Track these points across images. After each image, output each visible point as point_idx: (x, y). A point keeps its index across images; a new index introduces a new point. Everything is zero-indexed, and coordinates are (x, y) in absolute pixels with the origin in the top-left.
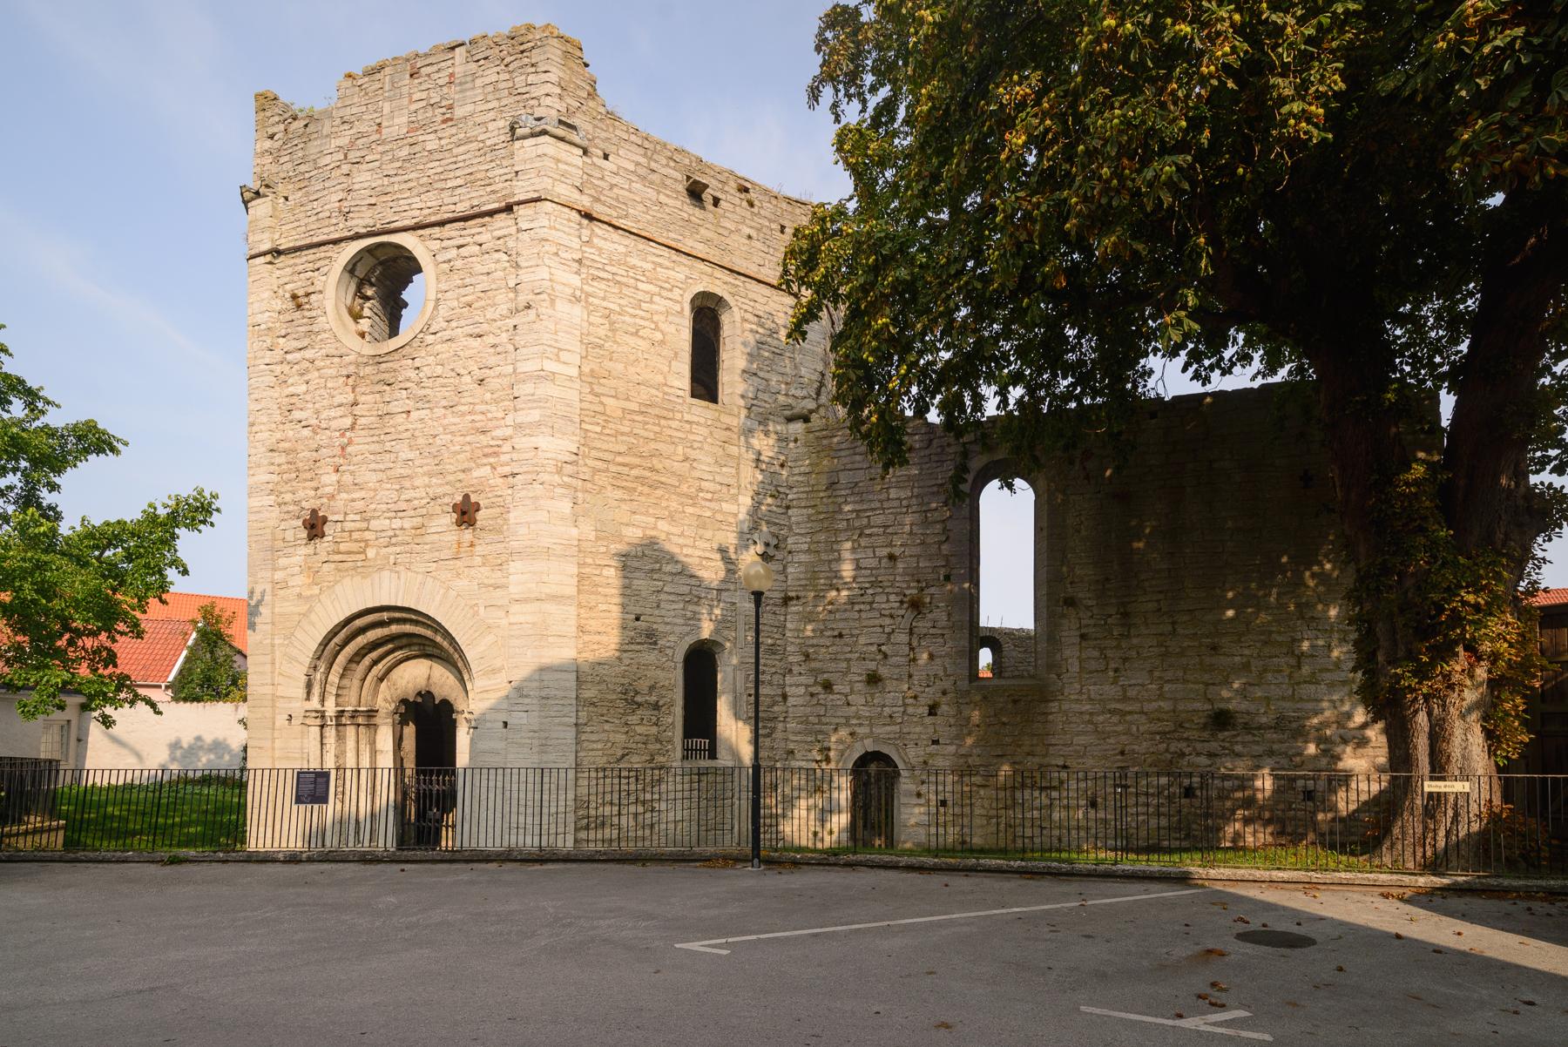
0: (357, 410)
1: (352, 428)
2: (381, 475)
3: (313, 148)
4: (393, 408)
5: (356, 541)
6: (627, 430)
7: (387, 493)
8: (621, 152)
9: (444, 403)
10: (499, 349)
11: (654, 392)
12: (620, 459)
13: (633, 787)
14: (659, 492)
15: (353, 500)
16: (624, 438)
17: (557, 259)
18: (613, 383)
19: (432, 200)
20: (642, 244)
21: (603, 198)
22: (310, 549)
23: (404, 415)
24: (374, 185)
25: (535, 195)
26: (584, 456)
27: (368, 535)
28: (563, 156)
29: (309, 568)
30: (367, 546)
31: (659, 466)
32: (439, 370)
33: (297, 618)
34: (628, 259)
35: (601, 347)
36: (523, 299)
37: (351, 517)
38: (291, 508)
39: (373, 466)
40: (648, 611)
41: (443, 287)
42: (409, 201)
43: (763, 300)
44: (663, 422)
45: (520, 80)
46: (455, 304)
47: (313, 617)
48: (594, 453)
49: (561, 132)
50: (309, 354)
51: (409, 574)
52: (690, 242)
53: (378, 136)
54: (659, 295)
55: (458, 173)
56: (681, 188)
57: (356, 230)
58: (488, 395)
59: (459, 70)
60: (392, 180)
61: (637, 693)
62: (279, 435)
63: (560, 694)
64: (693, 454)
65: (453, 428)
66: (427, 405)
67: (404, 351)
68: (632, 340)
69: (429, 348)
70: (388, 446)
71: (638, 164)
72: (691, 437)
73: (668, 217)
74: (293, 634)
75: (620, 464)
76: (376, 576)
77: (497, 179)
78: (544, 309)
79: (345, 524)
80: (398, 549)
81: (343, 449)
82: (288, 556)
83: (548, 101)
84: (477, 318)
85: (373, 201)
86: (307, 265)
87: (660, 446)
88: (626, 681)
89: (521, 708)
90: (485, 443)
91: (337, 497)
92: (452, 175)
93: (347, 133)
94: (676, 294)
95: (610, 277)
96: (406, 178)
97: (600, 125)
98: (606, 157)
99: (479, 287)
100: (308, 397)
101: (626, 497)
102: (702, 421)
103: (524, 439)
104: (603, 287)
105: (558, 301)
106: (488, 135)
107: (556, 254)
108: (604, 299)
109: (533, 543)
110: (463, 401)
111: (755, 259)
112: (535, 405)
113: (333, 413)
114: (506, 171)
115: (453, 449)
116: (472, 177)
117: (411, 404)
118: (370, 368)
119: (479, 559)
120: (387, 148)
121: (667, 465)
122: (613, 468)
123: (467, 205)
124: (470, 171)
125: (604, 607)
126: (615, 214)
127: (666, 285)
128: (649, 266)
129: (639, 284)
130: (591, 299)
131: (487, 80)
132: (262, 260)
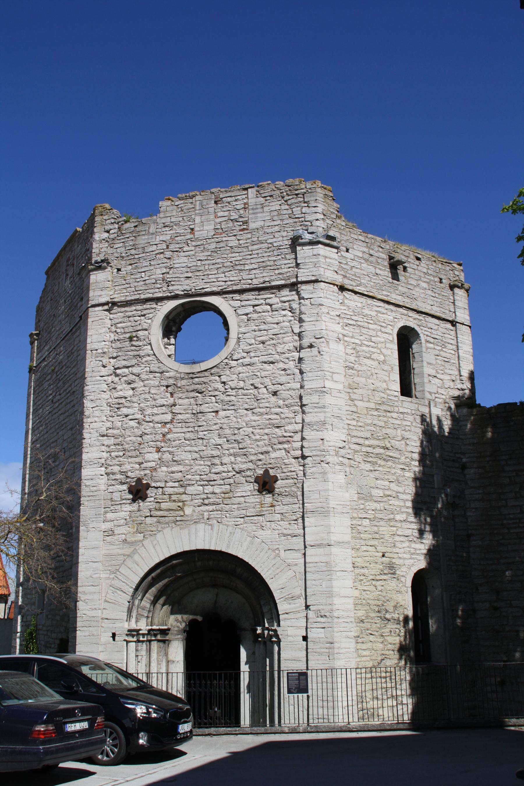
0: (176, 409)
1: (172, 421)
2: (196, 455)
3: (142, 240)
4: (204, 408)
5: (174, 501)
6: (370, 422)
7: (201, 467)
8: (355, 247)
9: (246, 406)
10: (288, 372)
11: (383, 395)
12: (367, 442)
13: (389, 685)
14: (390, 463)
15: (173, 472)
16: (369, 428)
17: (328, 316)
18: (360, 391)
19: (233, 276)
20: (370, 301)
21: (348, 275)
22: (135, 506)
23: (214, 414)
24: (189, 265)
25: (313, 278)
26: (349, 442)
27: (184, 497)
28: (328, 254)
29: (133, 521)
30: (184, 505)
31: (388, 445)
32: (242, 384)
33: (122, 558)
34: (363, 311)
35: (352, 368)
36: (306, 342)
37: (171, 484)
38: (118, 476)
39: (188, 448)
40: (390, 549)
41: (243, 330)
42: (217, 276)
43: (436, 327)
44: (388, 414)
45: (297, 211)
46: (253, 341)
47: (136, 557)
48: (354, 440)
49: (327, 241)
50: (136, 370)
51: (221, 526)
52: (394, 296)
53: (192, 236)
54: (381, 331)
55: (253, 261)
56: (386, 263)
57: (177, 292)
58: (281, 402)
59: (252, 201)
60: (203, 263)
61: (387, 611)
62: (109, 424)
63: (345, 614)
64: (407, 435)
65: (254, 424)
66: (232, 408)
67: (213, 371)
68: (369, 362)
69: (232, 369)
70: (201, 435)
71: (364, 252)
72: (405, 423)
73: (381, 282)
74: (118, 570)
75: (369, 446)
76: (193, 527)
77: (283, 266)
78: (323, 347)
79: (165, 489)
80: (211, 508)
81: (164, 436)
82: (115, 511)
83: (318, 223)
84: (270, 351)
85: (189, 275)
86: (135, 312)
87: (388, 431)
88: (380, 603)
89: (318, 625)
90: (280, 434)
91: (159, 470)
92: (248, 262)
93: (168, 232)
94: (388, 330)
95: (354, 323)
96: (214, 261)
97: (343, 232)
98: (347, 251)
99: (271, 332)
100: (135, 399)
101: (372, 469)
102: (409, 411)
103: (312, 433)
104: (352, 330)
105: (330, 342)
106: (274, 240)
107: (328, 313)
108: (352, 337)
109: (324, 504)
110: (261, 405)
111: (429, 302)
112: (319, 410)
113: (155, 410)
114: (289, 262)
115: (254, 437)
116: (264, 264)
117: (219, 407)
118: (185, 381)
119: (279, 515)
120: (199, 243)
121: (393, 444)
122: (364, 449)
123: (262, 280)
124: (262, 260)
125: (364, 548)
126: (354, 284)
127: (384, 325)
128: (374, 314)
129: (370, 325)
130: (346, 338)
131: (273, 208)
132: (100, 308)
